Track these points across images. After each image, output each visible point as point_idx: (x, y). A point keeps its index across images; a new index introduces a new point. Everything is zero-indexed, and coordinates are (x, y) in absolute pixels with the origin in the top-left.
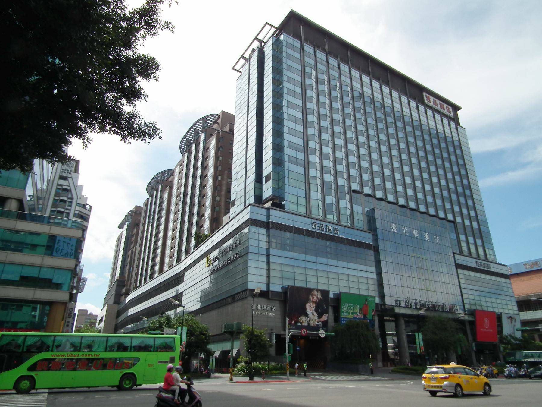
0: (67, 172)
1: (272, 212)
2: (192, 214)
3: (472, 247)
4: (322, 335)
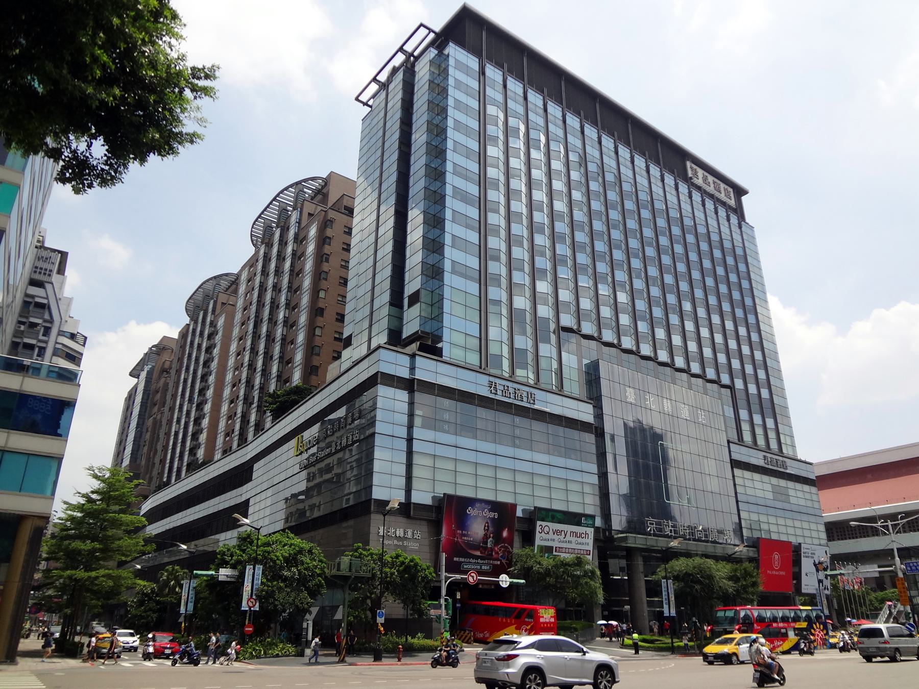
0: (43, 272)
1: (419, 361)
2: (269, 357)
3: (759, 431)
4: (504, 583)
